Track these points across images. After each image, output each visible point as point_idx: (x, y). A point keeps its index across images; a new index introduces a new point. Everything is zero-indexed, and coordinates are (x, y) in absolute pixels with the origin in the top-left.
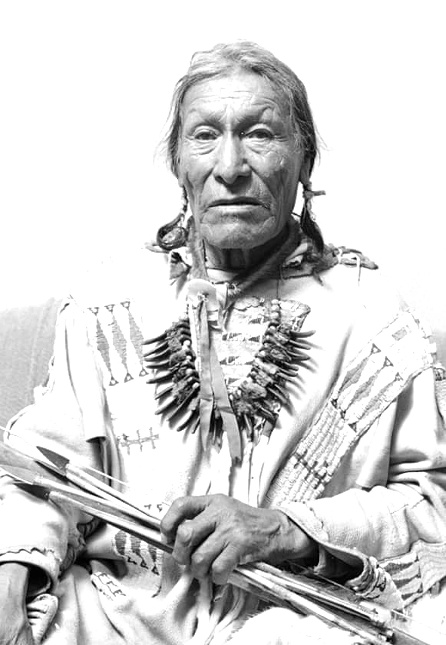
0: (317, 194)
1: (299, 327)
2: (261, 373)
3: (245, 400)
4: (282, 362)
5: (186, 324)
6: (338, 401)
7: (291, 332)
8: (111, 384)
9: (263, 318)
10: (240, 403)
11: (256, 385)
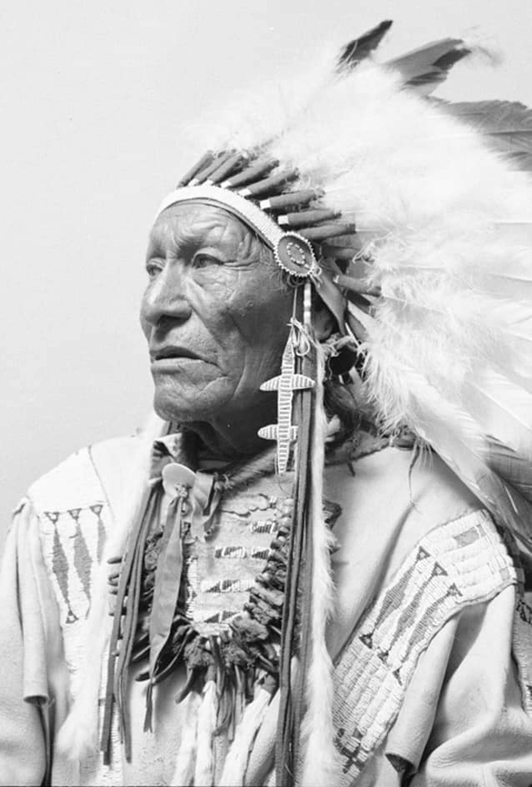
2: (261, 604)
6: (373, 637)
8: (68, 621)
10: (229, 649)
11: (254, 622)
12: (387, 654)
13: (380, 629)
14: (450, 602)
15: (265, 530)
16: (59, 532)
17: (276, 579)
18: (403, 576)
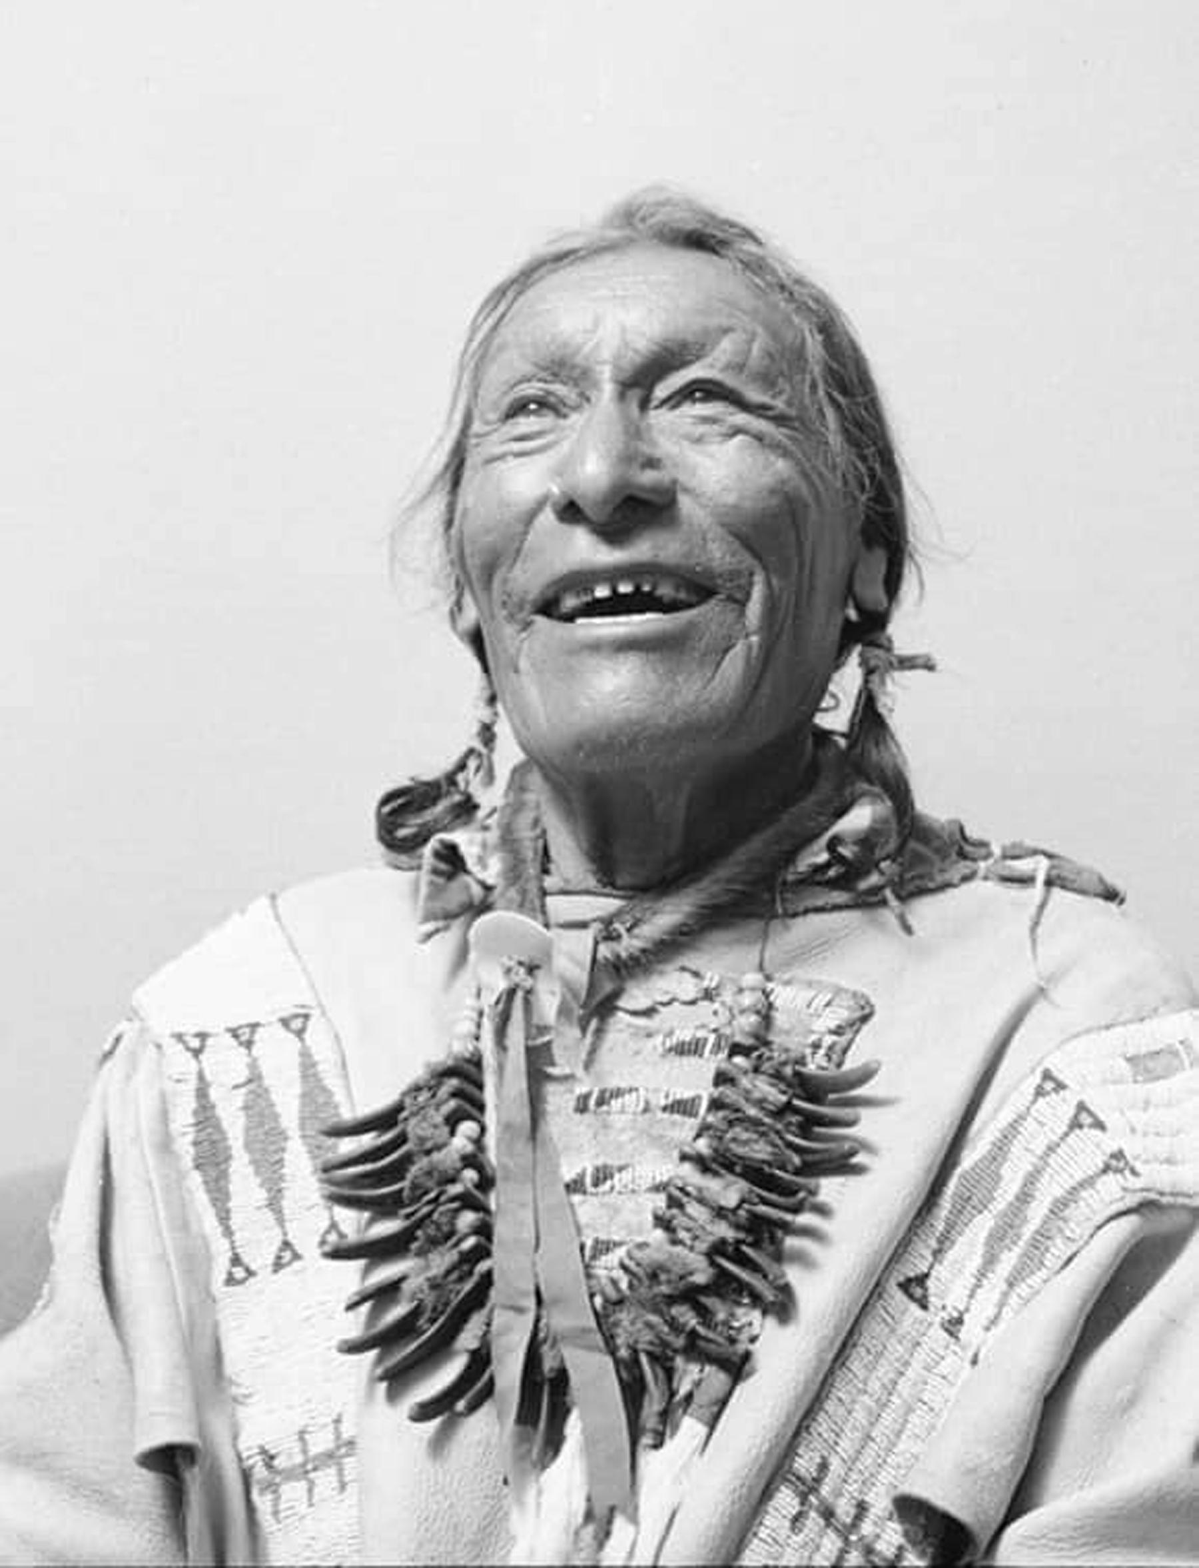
0: (907, 663)
2: (693, 1209)
3: (642, 1304)
4: (766, 1169)
5: (472, 1069)
6: (930, 1283)
7: (797, 1074)
8: (231, 1280)
9: (712, 1038)
10: (624, 1316)
11: (678, 1249)
12: (959, 1321)
13: (945, 1263)
14: (1111, 1185)
15: (690, 1049)
16: (208, 1077)
17: (728, 1150)
18: (998, 1135)
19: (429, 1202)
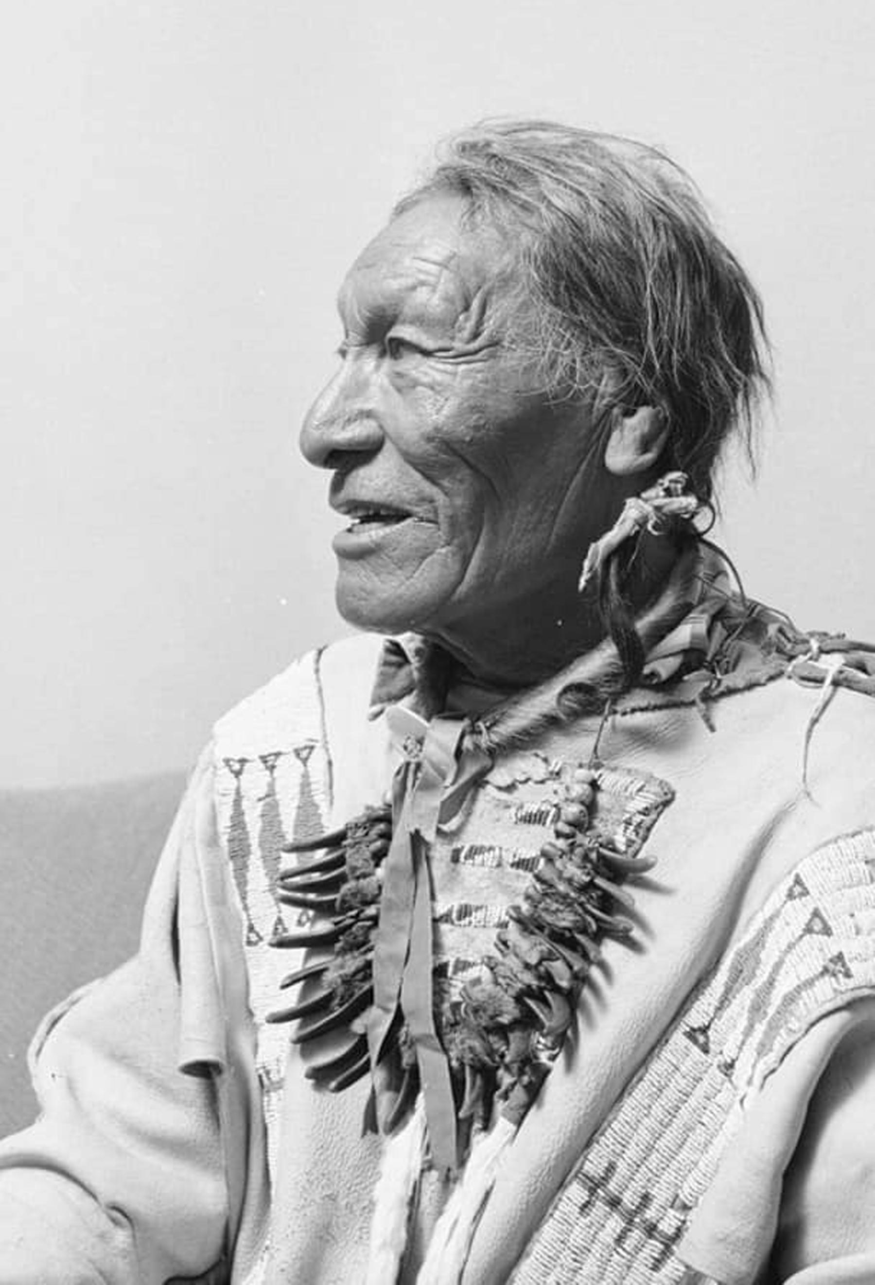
1: (639, 841)
12: (731, 1066)
17: (540, 916)
19: (352, 917)
